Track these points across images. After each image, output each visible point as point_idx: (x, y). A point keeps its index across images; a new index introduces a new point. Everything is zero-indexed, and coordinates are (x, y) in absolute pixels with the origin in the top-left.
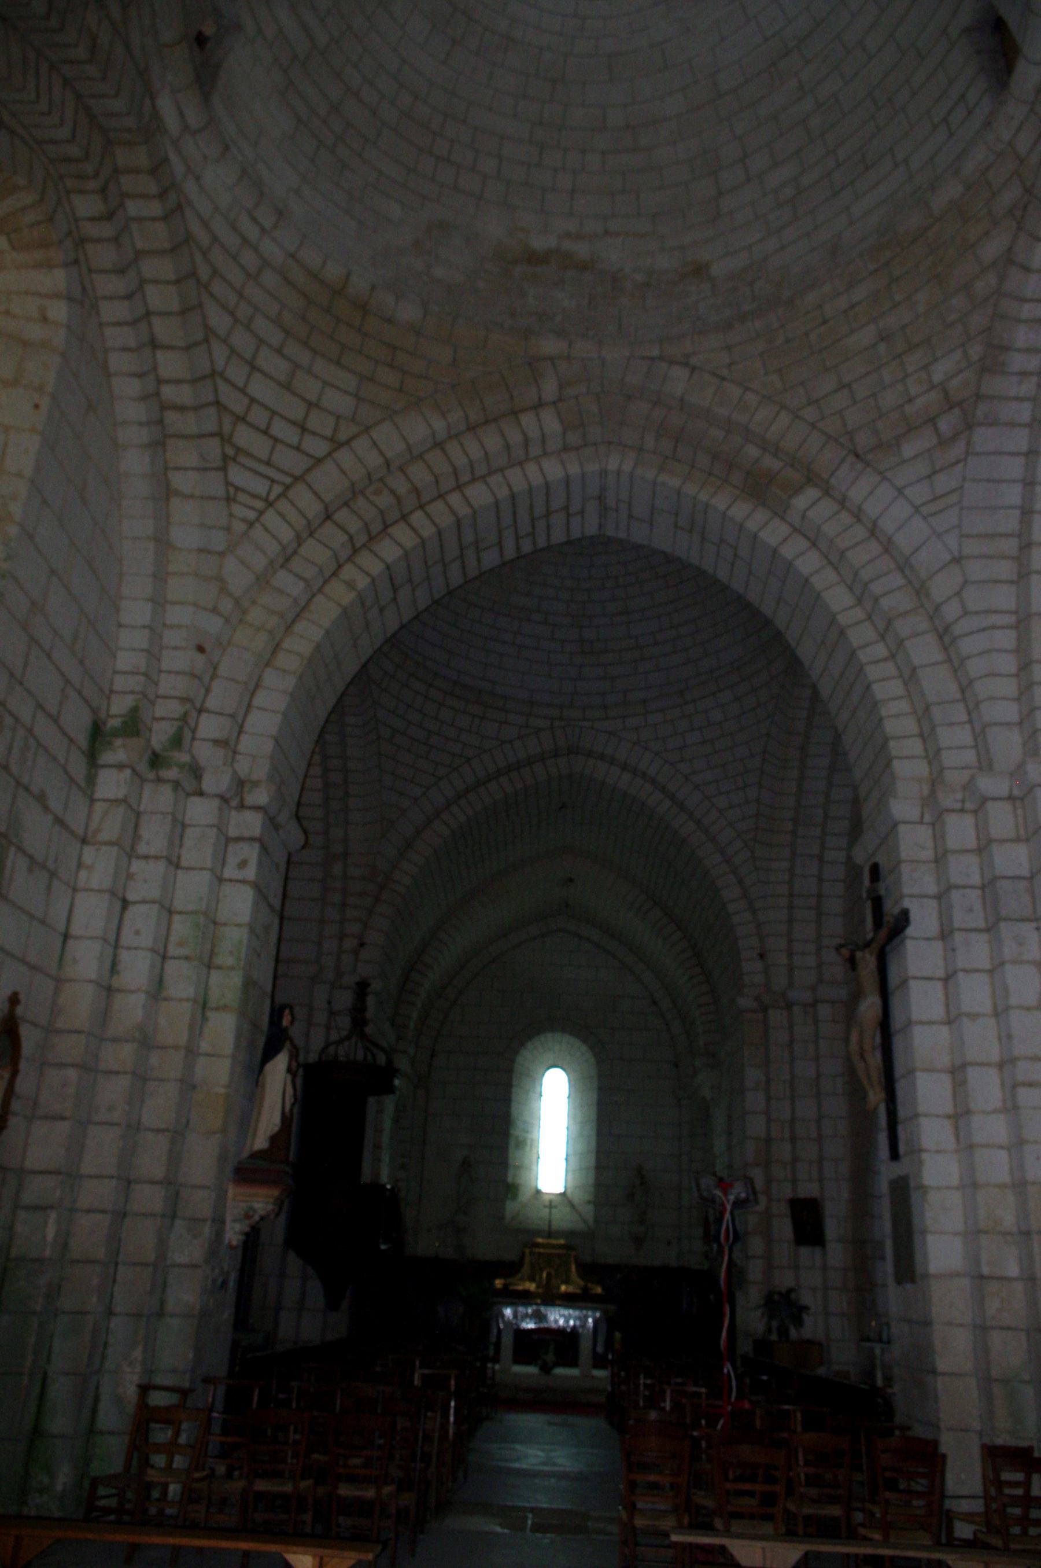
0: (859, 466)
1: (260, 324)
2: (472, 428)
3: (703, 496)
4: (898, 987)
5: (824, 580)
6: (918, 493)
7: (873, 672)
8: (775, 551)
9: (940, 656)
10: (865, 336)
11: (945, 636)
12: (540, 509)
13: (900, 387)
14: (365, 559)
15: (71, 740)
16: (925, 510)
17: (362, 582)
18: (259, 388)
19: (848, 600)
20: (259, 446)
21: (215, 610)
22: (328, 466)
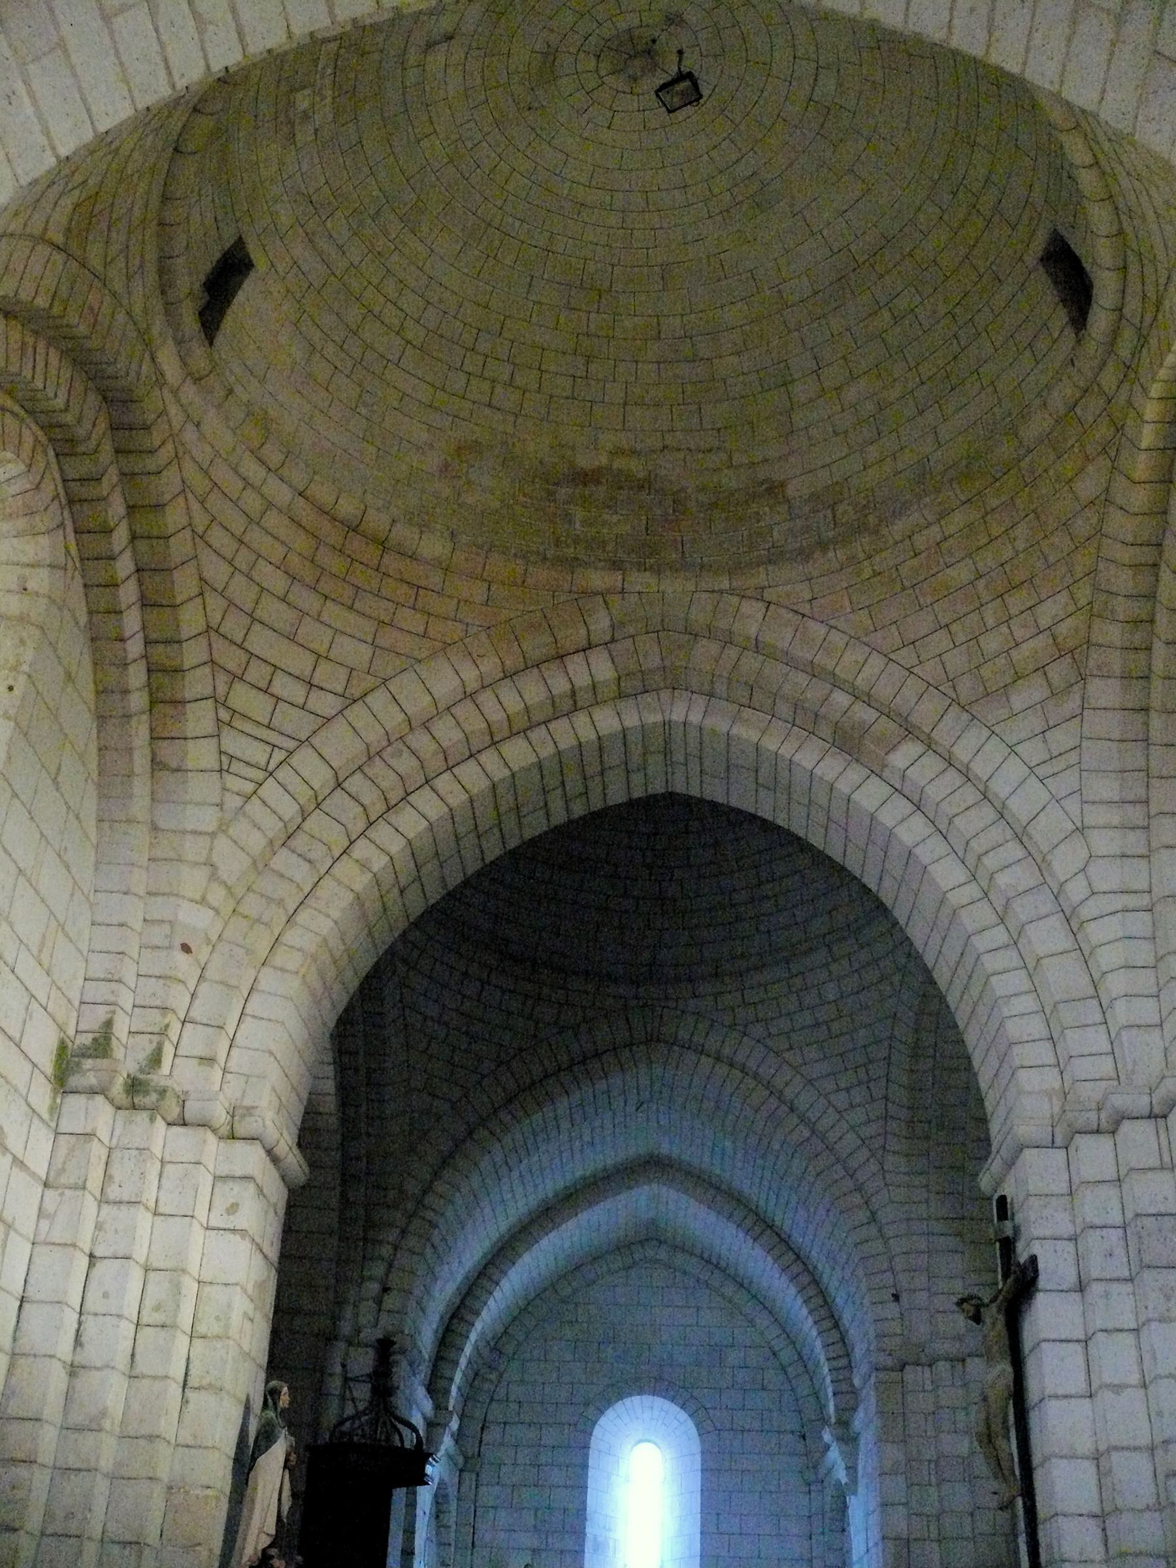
0: (965, 716)
1: (264, 570)
2: (509, 675)
3: (786, 751)
4: (1031, 1351)
5: (931, 850)
6: (1033, 751)
7: (991, 963)
8: (872, 817)
9: (1068, 944)
10: (961, 573)
11: (1071, 920)
12: (593, 769)
13: (1004, 629)
14: (382, 833)
15: (35, 1065)
16: (1041, 771)
17: (379, 862)
18: (260, 642)
19: (961, 875)
20: (258, 706)
21: (203, 901)
22: (339, 728)
